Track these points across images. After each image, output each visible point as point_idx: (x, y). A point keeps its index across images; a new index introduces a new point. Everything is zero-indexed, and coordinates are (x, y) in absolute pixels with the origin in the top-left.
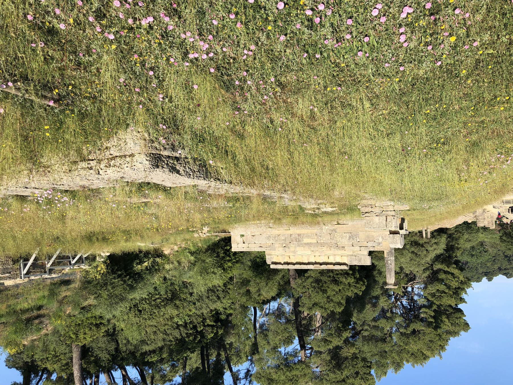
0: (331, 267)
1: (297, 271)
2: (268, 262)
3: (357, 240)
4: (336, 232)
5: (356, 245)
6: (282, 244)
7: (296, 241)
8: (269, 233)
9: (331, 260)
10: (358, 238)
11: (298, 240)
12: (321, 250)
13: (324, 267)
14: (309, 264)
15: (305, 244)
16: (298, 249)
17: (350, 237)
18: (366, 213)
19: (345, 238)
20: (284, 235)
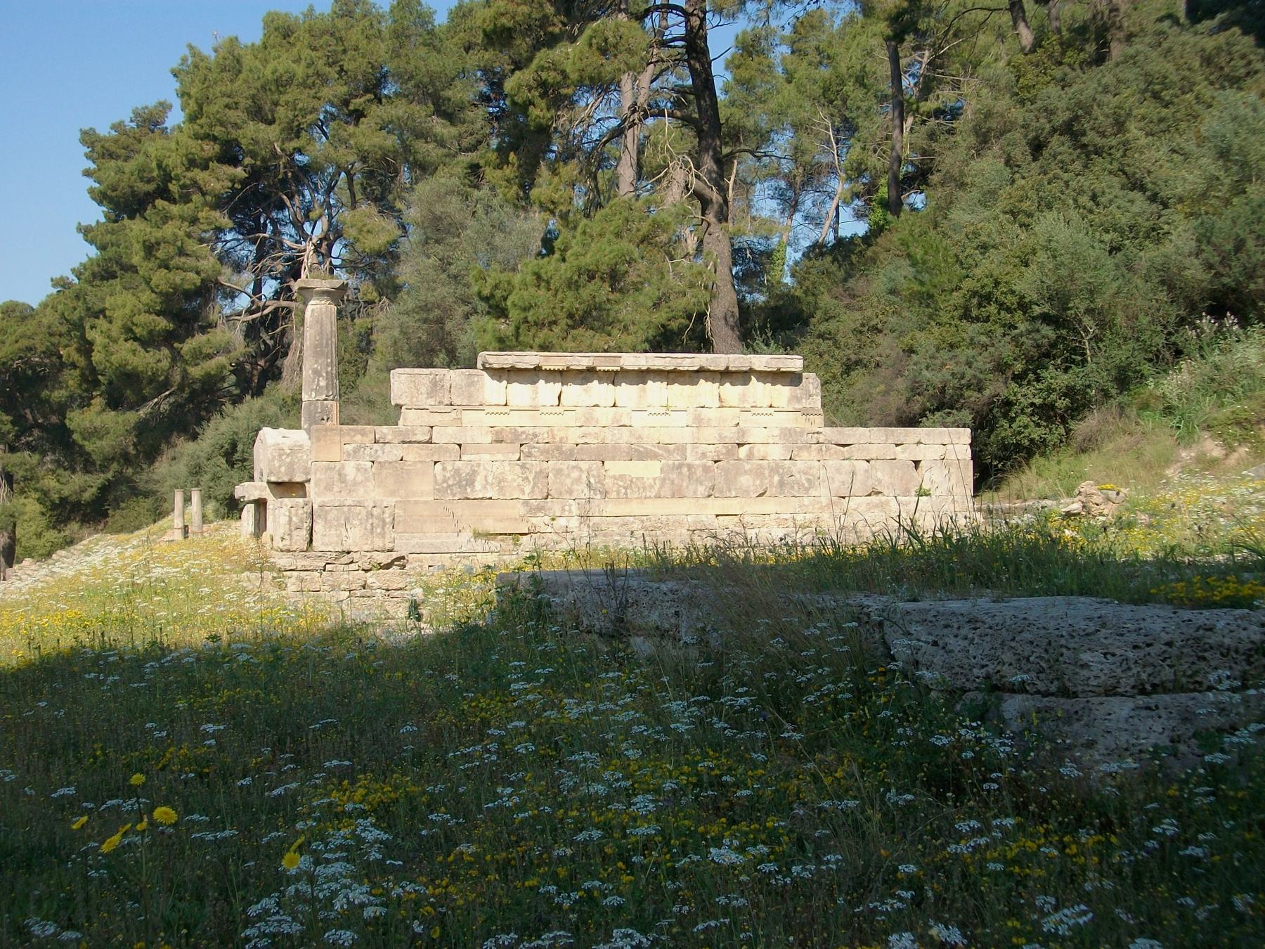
0: (604, 362)
1: (703, 344)
2: (812, 382)
3: (444, 469)
4: (526, 503)
5: (447, 451)
6: (750, 457)
7: (690, 467)
8: (806, 501)
9: (546, 390)
10: (439, 478)
11: (685, 470)
12: (591, 430)
13: (529, 359)
14: (642, 376)
15: (653, 456)
16: (686, 436)
17: (471, 482)
18: (388, 566)
19: (490, 479)
20: (745, 493)
